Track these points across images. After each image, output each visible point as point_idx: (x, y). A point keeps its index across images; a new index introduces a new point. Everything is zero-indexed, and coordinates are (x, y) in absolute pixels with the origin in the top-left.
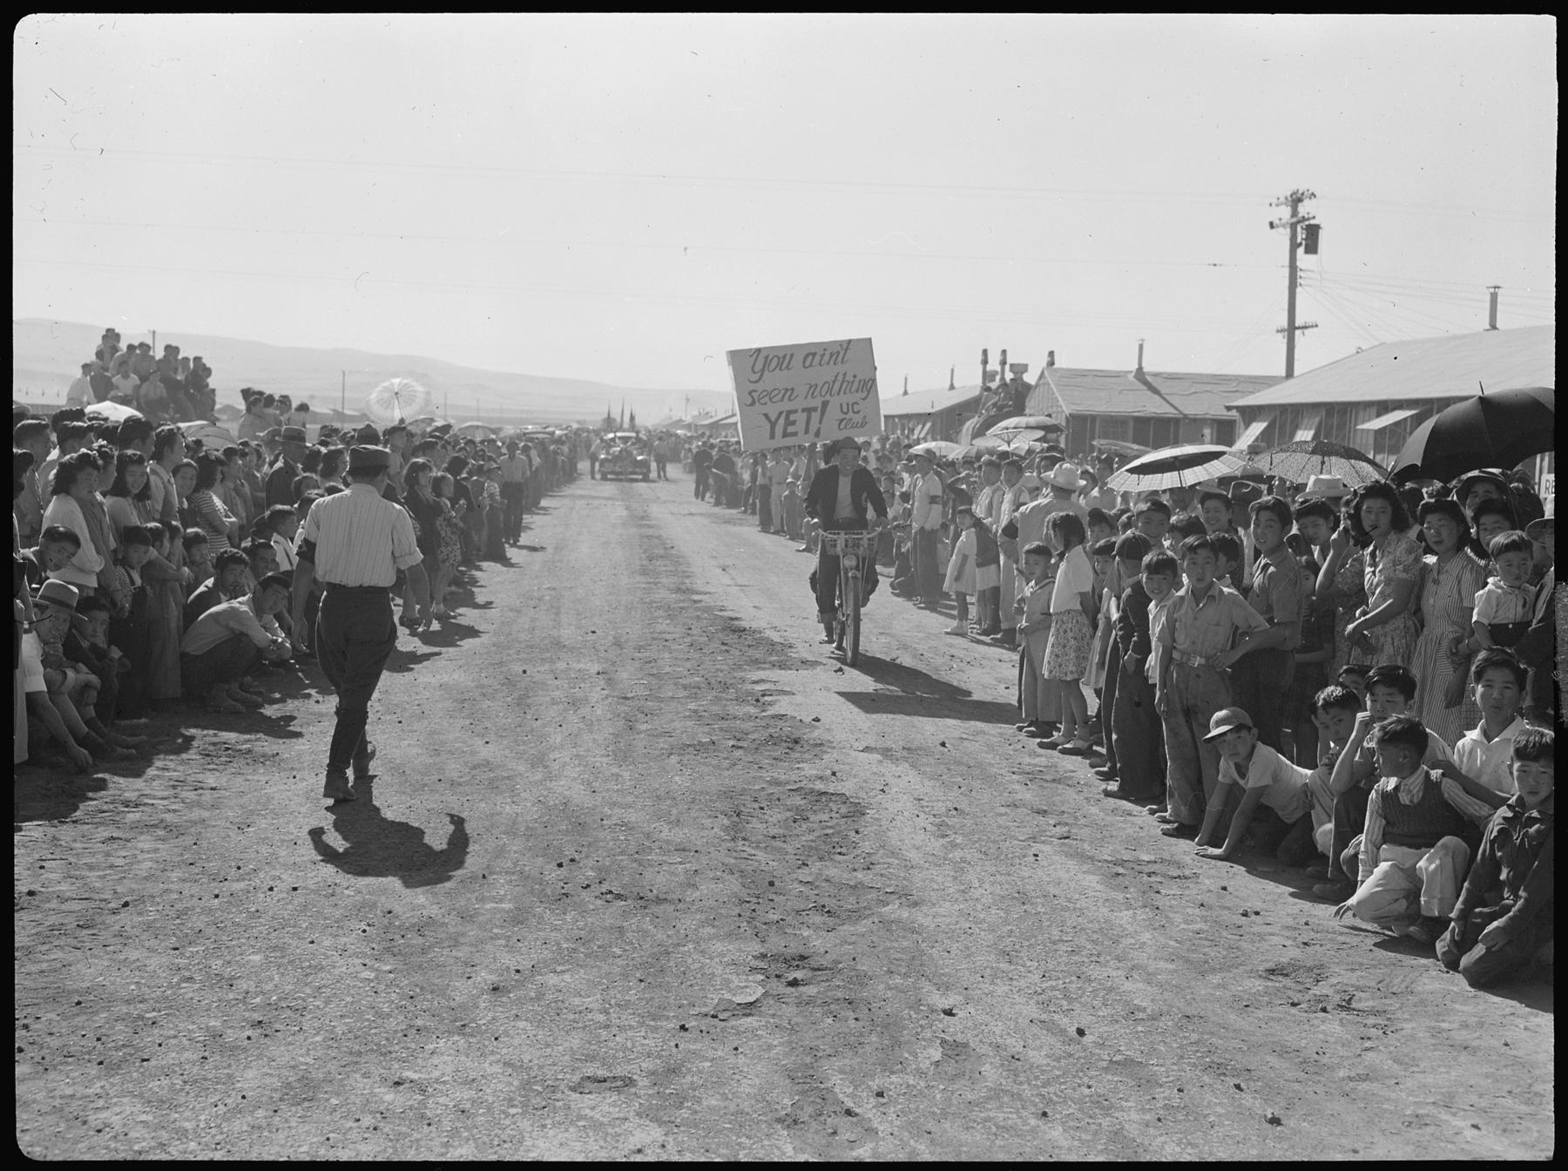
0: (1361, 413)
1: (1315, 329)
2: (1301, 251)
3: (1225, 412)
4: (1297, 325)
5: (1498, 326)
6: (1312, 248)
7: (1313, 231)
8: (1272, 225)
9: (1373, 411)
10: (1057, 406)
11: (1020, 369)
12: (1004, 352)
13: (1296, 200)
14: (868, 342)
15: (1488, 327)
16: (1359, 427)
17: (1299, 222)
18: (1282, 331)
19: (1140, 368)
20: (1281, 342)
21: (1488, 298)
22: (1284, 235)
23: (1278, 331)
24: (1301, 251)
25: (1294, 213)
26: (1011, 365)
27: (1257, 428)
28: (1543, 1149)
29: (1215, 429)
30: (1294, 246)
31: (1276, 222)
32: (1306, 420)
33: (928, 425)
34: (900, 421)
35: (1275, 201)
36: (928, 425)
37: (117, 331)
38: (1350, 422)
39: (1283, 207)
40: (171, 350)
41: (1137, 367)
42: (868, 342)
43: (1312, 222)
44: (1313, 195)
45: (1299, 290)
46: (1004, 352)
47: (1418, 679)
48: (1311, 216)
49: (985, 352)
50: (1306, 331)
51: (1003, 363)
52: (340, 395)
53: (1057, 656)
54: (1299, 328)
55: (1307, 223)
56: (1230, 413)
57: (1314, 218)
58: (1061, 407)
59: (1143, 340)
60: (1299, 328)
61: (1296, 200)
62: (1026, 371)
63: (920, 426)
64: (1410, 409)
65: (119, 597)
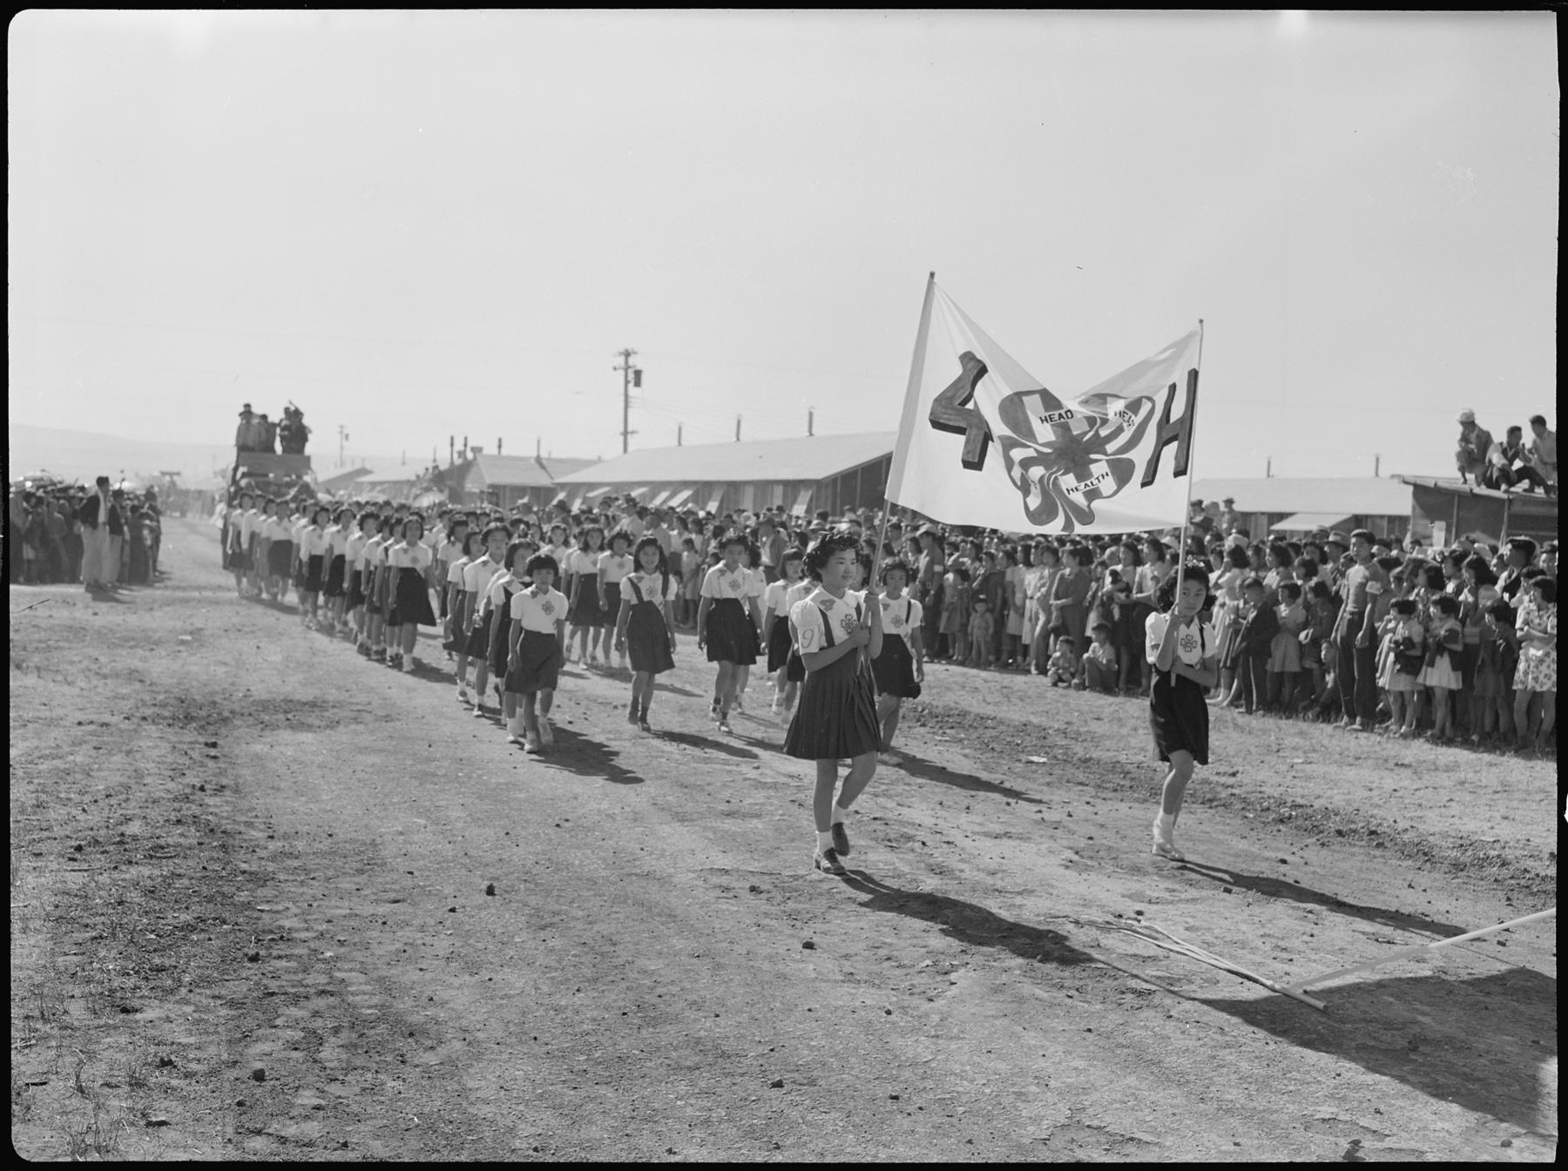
2: (631, 386)
6: (638, 383)
7: (638, 374)
14: (980, 469)
20: (622, 438)
22: (622, 372)
24: (631, 386)
30: (627, 382)
42: (980, 469)
47: (1344, 597)
61: (627, 354)
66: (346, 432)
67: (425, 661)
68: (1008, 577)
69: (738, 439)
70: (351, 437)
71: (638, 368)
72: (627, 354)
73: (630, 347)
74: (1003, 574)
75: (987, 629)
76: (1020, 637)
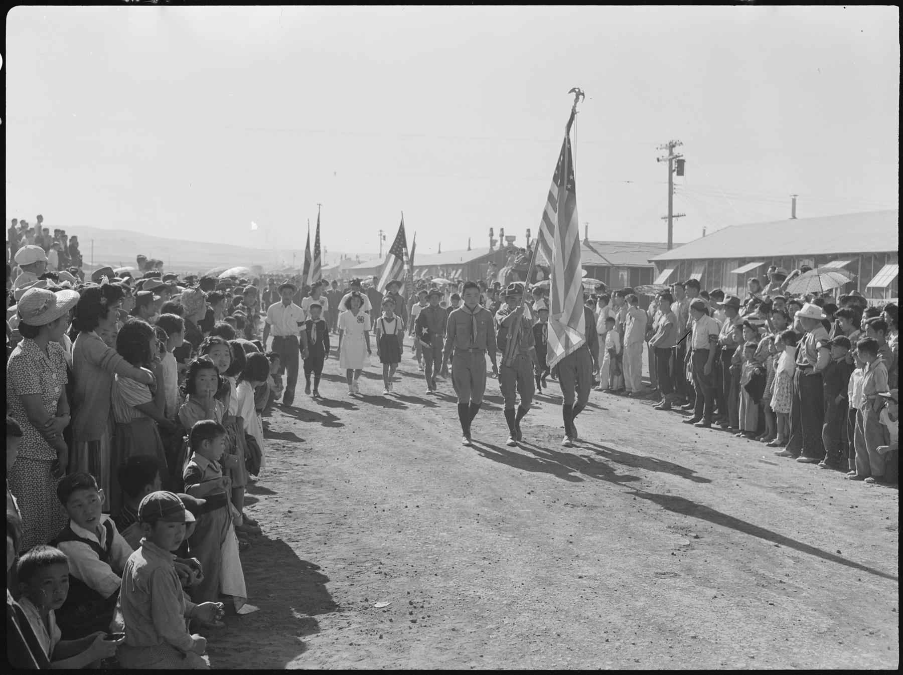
0: (729, 265)
1: (684, 217)
2: (675, 174)
3: (647, 263)
4: (673, 215)
5: (796, 216)
6: (681, 172)
7: (681, 163)
8: (658, 160)
9: (736, 264)
10: (542, 260)
11: (511, 239)
12: (502, 229)
13: (672, 146)
15: (791, 217)
16: (732, 272)
17: (673, 158)
19: (586, 239)
21: (791, 201)
22: (665, 166)
23: (662, 218)
24: (675, 174)
25: (671, 153)
26: (506, 237)
27: (668, 272)
28: (893, 664)
29: (629, 272)
30: (671, 172)
31: (661, 158)
32: (696, 268)
33: (460, 271)
34: (441, 268)
35: (659, 147)
36: (460, 271)
37: (26, 222)
38: (723, 269)
39: (664, 150)
41: (584, 238)
43: (681, 158)
44: (682, 143)
45: (674, 195)
46: (502, 229)
48: (680, 155)
49: (491, 229)
50: (679, 218)
51: (502, 235)
52: (91, 254)
53: (778, 400)
54: (675, 216)
55: (678, 159)
56: (651, 264)
57: (682, 156)
58: (545, 260)
59: (587, 223)
60: (675, 216)
61: (672, 146)
62: (515, 240)
63: (454, 272)
64: (760, 262)
66: (383, 234)
67: (79, 248)
70: (386, 238)
72: (381, 231)
73: (675, 139)
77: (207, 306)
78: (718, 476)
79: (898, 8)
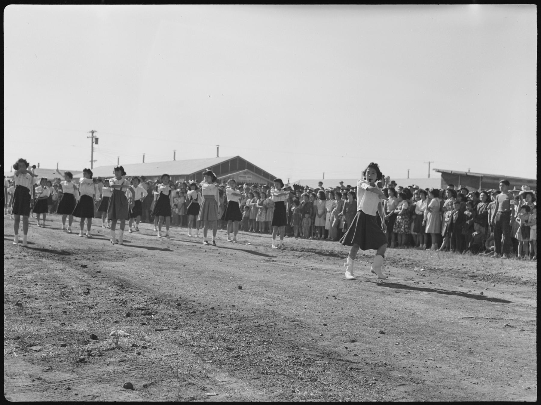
2: (94, 144)
6: (97, 143)
7: (97, 140)
8: (88, 137)
18: (469, 171)
20: (90, 163)
22: (91, 139)
24: (94, 144)
25: (92, 135)
30: (93, 143)
31: (89, 137)
40: (452, 172)
59: (218, 146)
61: (93, 132)
65: (392, 372)
68: (315, 204)
69: (175, 160)
71: (97, 137)
72: (93, 132)
73: (94, 130)
74: (312, 203)
75: (308, 224)
76: (324, 227)
77: (132, 232)
78: (133, 241)
79: (536, 5)
